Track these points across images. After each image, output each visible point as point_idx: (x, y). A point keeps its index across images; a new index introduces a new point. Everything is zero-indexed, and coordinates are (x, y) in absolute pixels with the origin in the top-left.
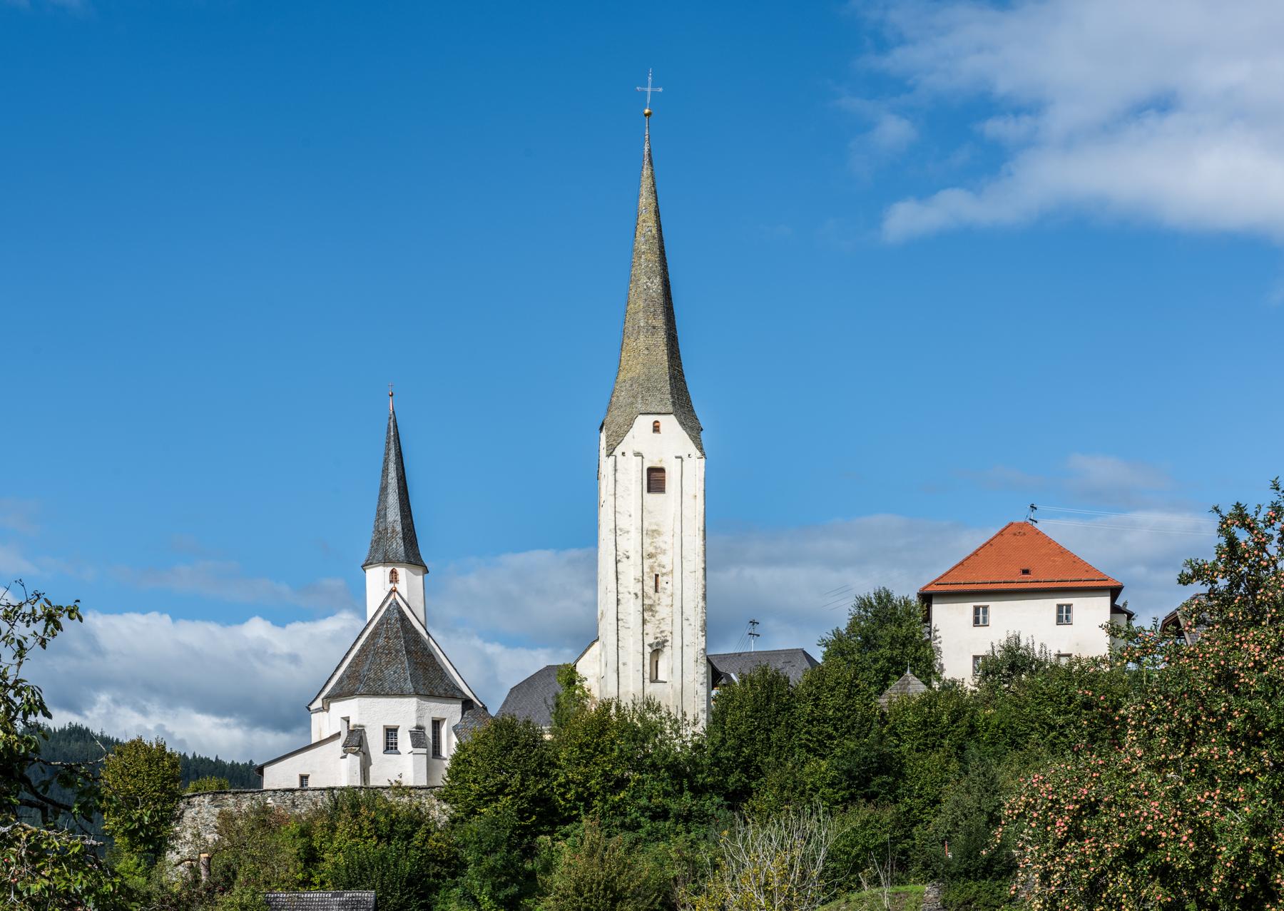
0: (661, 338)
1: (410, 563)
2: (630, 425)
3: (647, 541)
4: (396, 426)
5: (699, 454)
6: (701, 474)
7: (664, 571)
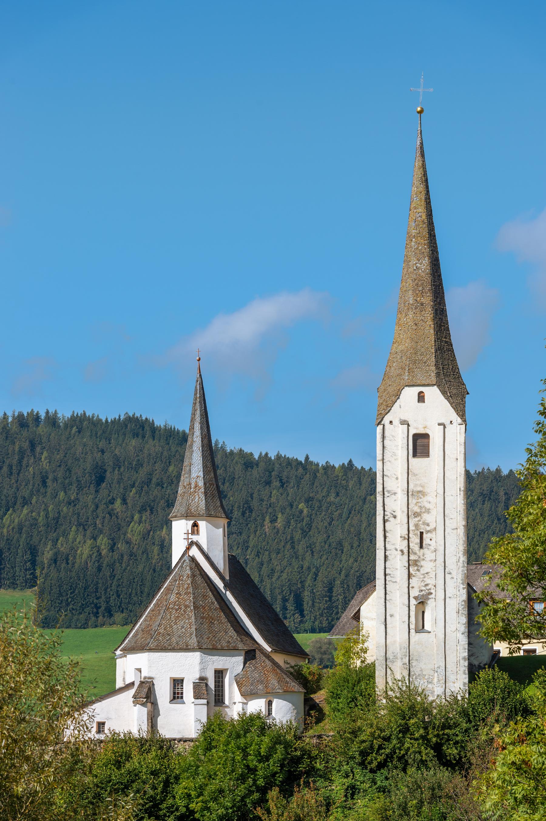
0: (428, 315)
1: (210, 516)
2: (398, 396)
3: (412, 501)
4: (202, 388)
5: (459, 420)
6: (461, 438)
7: (428, 528)
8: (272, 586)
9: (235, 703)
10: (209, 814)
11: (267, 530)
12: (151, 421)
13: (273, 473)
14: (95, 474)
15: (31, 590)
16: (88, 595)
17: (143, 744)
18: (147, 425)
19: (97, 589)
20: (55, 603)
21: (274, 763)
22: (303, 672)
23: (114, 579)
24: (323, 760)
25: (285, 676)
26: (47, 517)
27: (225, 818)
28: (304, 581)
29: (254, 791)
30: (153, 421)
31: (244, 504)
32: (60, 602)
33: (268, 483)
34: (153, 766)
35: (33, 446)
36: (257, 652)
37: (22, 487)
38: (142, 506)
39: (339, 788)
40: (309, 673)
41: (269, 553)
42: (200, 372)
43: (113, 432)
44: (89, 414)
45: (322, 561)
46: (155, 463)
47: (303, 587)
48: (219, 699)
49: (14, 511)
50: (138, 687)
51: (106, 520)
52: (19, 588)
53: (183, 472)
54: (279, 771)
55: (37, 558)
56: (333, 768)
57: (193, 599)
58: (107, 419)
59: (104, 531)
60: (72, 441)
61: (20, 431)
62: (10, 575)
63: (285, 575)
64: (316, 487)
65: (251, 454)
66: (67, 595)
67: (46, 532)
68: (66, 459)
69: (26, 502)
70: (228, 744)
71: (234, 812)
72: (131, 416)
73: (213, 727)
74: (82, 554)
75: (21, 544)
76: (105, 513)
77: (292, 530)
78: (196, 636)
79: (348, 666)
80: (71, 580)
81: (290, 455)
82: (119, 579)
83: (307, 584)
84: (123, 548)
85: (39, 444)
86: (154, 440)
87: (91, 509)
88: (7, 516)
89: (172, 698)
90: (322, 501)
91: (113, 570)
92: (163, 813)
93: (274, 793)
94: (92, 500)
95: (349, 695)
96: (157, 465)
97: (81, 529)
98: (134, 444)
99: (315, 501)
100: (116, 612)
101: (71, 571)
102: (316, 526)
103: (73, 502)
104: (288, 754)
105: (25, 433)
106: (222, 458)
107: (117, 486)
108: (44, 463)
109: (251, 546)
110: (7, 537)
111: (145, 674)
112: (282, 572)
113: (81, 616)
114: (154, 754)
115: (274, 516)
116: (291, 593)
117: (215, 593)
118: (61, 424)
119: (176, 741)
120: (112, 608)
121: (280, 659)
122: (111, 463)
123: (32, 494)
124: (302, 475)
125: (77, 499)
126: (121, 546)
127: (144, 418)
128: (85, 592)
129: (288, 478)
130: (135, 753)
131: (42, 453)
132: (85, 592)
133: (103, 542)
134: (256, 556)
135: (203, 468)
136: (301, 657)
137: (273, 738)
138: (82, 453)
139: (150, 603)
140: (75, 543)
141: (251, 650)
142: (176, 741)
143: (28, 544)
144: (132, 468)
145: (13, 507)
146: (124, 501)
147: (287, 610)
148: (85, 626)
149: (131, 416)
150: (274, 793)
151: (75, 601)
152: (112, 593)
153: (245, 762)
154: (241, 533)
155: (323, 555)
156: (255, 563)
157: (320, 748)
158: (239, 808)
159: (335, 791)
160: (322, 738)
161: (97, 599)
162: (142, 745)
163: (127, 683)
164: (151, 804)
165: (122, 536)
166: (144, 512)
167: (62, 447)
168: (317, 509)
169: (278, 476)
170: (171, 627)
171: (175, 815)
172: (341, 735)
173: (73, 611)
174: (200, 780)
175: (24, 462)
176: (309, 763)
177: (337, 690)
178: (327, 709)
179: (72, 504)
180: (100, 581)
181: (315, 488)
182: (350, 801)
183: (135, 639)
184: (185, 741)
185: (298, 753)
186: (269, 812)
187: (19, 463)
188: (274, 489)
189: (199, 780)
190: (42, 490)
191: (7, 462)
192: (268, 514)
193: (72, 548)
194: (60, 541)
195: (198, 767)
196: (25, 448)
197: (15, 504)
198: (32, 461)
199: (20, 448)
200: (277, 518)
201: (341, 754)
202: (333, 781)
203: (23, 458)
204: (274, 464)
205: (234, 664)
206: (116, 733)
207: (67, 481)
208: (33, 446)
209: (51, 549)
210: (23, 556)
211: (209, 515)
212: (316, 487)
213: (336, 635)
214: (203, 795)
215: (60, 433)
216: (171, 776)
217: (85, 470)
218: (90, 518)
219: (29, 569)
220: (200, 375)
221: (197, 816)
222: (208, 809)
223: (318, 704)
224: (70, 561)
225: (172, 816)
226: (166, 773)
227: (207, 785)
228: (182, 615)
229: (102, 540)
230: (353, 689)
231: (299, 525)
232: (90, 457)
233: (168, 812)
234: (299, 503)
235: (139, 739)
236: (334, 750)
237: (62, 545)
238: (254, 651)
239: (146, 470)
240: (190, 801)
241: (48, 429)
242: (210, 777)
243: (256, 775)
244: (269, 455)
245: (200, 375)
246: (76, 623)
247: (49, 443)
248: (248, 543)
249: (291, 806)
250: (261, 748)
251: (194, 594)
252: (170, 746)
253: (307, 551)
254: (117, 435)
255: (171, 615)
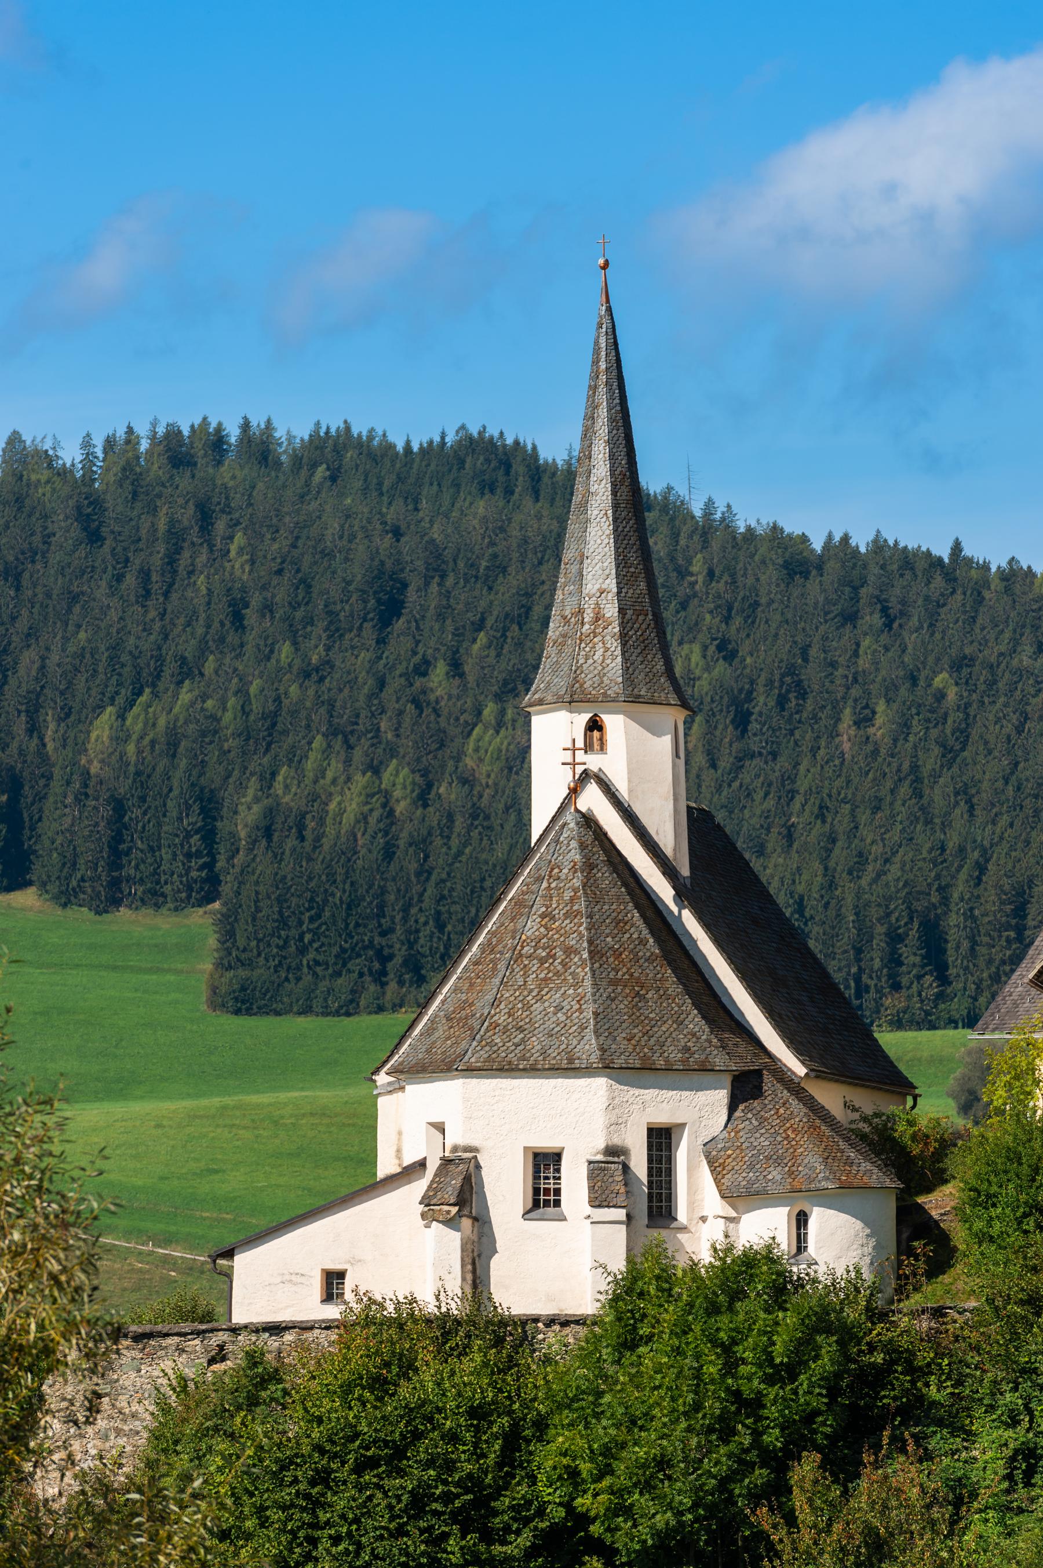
1: (635, 699)
8: (859, 899)
9: (704, 1219)
10: (629, 1524)
11: (846, 746)
12: (529, 447)
13: (863, 591)
14: (375, 593)
15: (201, 911)
16: (357, 925)
17: (449, 1333)
18: (519, 459)
19: (381, 907)
20: (269, 945)
21: (812, 1385)
22: (896, 1135)
23: (428, 879)
24: (949, 1378)
25: (842, 1145)
26: (245, 712)
27: (674, 1538)
28: (948, 886)
29: (755, 1463)
30: (534, 448)
31: (783, 676)
32: (281, 943)
33: (850, 618)
34: (474, 1392)
35: (205, 517)
36: (767, 1077)
37: (176, 631)
38: (505, 683)
39: (990, 1454)
40: (914, 1137)
41: (853, 810)
42: (608, 301)
43: (427, 479)
44: (359, 428)
45: (998, 831)
46: (540, 563)
47: (945, 901)
48: (659, 1206)
49: (155, 695)
50: (436, 1175)
51: (407, 721)
52: (171, 906)
53: (562, 580)
54: (824, 1408)
55: (219, 824)
56: (973, 1400)
57: (588, 929)
58: (408, 443)
59: (401, 751)
60: (314, 505)
61: (172, 477)
62: (146, 869)
63: (894, 870)
64: (983, 629)
65: (804, 539)
66: (300, 923)
67: (244, 753)
68: (295, 553)
69: (187, 671)
70: (685, 1333)
71: (697, 1520)
72: (475, 435)
73: (640, 1283)
74: (342, 812)
75: (175, 783)
76: (404, 699)
77: (915, 747)
78: (595, 1032)
79: (1018, 1116)
80: (312, 884)
81: (910, 541)
82: (443, 881)
83: (956, 895)
84: (453, 797)
85: (223, 511)
86: (537, 500)
87: (366, 690)
88: (136, 710)
89: (530, 1205)
90: (998, 666)
91: (426, 857)
92: (502, 1522)
93: (806, 1469)
94: (367, 665)
95: (1023, 1197)
96: (544, 567)
97: (338, 743)
98: (481, 511)
99: (976, 669)
100: (434, 970)
101: (310, 859)
102: (981, 737)
103: (317, 670)
104: (850, 1360)
105: (184, 482)
106: (724, 549)
107: (437, 627)
108: (238, 565)
109: (802, 791)
110: (136, 765)
111: (455, 1137)
112: (887, 861)
113: (340, 981)
114: (478, 1358)
115: (867, 706)
116: (911, 919)
117: (650, 913)
118: (284, 458)
119: (540, 1325)
120: (423, 960)
121: (831, 1097)
122: (419, 564)
123: (203, 650)
124: (942, 595)
125: (328, 662)
126: (447, 791)
127: (509, 441)
128: (348, 915)
129: (903, 602)
130: (425, 1355)
131: (231, 538)
132: (348, 915)
133: (398, 778)
134: (817, 817)
135: (617, 566)
136: (893, 1092)
137: (808, 1315)
138: (341, 537)
139: (470, 942)
140: (322, 781)
141: (750, 1071)
142: (540, 1325)
143: (193, 785)
144: (476, 577)
145: (154, 685)
146: (456, 667)
147: (901, 964)
148: (349, 1009)
149: (475, 435)
150: (806, 1469)
151: (322, 939)
152: (422, 920)
153: (730, 1381)
154: (774, 755)
155: (1001, 814)
156: (812, 838)
157: (939, 1344)
158: (712, 1508)
159: (980, 1464)
160: (945, 1315)
161: (383, 934)
162: (446, 1335)
163: (407, 1161)
164: (470, 1497)
165: (451, 763)
166: (510, 696)
167: (287, 519)
168: (983, 687)
169: (877, 597)
170: (527, 1007)
171: (536, 1528)
172: (997, 1309)
173: (318, 969)
174: (604, 1430)
175: (184, 560)
176: (907, 1385)
177: (990, 1183)
178: (959, 1236)
179: (315, 677)
180: (391, 886)
181: (978, 631)
182: (1022, 1492)
183: (429, 1041)
184: (565, 1323)
185: (879, 1358)
186: (791, 1520)
187: (168, 563)
188: (866, 634)
189: (601, 1431)
190: (232, 638)
191: (137, 562)
192: (850, 702)
193: (314, 798)
194: (280, 778)
195: (600, 1394)
196: (186, 523)
197: (158, 677)
198: (202, 558)
199: (172, 523)
200: (874, 713)
201: (994, 1359)
202: (975, 1435)
203: (178, 550)
204: (865, 566)
205: (702, 1111)
206: (375, 1302)
207: (299, 614)
208: (205, 517)
209: (257, 800)
210: (180, 819)
211: (634, 697)
212: (983, 629)
213: (994, 1030)
214: (612, 1473)
215: (280, 483)
216: (525, 1420)
217: (349, 583)
218: (363, 714)
219: (198, 854)
220: (609, 310)
221: (596, 1529)
222: (627, 1511)
223: (936, 1222)
224: (308, 834)
225: (527, 1530)
226: (510, 1413)
227: (623, 1446)
228: (557, 974)
229: (397, 775)
230: (1034, 1180)
231: (934, 733)
232: (361, 548)
233: (514, 1519)
234: (935, 673)
235: (437, 1318)
236: (977, 1349)
237: (287, 787)
238: (758, 1073)
239: (515, 582)
240: (575, 1488)
241: (246, 471)
242: (634, 1422)
243: (759, 1419)
244: (853, 542)
245: (609, 310)
246: (326, 1000)
247: (250, 510)
248: (794, 782)
249: (853, 1503)
250: (774, 1344)
251: (590, 916)
252: (525, 1337)
253: (957, 803)
254: (435, 487)
255: (526, 975)
